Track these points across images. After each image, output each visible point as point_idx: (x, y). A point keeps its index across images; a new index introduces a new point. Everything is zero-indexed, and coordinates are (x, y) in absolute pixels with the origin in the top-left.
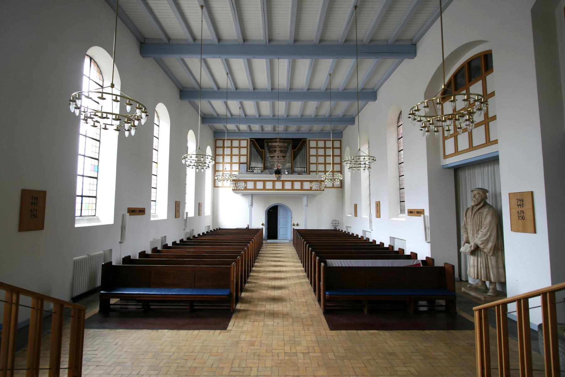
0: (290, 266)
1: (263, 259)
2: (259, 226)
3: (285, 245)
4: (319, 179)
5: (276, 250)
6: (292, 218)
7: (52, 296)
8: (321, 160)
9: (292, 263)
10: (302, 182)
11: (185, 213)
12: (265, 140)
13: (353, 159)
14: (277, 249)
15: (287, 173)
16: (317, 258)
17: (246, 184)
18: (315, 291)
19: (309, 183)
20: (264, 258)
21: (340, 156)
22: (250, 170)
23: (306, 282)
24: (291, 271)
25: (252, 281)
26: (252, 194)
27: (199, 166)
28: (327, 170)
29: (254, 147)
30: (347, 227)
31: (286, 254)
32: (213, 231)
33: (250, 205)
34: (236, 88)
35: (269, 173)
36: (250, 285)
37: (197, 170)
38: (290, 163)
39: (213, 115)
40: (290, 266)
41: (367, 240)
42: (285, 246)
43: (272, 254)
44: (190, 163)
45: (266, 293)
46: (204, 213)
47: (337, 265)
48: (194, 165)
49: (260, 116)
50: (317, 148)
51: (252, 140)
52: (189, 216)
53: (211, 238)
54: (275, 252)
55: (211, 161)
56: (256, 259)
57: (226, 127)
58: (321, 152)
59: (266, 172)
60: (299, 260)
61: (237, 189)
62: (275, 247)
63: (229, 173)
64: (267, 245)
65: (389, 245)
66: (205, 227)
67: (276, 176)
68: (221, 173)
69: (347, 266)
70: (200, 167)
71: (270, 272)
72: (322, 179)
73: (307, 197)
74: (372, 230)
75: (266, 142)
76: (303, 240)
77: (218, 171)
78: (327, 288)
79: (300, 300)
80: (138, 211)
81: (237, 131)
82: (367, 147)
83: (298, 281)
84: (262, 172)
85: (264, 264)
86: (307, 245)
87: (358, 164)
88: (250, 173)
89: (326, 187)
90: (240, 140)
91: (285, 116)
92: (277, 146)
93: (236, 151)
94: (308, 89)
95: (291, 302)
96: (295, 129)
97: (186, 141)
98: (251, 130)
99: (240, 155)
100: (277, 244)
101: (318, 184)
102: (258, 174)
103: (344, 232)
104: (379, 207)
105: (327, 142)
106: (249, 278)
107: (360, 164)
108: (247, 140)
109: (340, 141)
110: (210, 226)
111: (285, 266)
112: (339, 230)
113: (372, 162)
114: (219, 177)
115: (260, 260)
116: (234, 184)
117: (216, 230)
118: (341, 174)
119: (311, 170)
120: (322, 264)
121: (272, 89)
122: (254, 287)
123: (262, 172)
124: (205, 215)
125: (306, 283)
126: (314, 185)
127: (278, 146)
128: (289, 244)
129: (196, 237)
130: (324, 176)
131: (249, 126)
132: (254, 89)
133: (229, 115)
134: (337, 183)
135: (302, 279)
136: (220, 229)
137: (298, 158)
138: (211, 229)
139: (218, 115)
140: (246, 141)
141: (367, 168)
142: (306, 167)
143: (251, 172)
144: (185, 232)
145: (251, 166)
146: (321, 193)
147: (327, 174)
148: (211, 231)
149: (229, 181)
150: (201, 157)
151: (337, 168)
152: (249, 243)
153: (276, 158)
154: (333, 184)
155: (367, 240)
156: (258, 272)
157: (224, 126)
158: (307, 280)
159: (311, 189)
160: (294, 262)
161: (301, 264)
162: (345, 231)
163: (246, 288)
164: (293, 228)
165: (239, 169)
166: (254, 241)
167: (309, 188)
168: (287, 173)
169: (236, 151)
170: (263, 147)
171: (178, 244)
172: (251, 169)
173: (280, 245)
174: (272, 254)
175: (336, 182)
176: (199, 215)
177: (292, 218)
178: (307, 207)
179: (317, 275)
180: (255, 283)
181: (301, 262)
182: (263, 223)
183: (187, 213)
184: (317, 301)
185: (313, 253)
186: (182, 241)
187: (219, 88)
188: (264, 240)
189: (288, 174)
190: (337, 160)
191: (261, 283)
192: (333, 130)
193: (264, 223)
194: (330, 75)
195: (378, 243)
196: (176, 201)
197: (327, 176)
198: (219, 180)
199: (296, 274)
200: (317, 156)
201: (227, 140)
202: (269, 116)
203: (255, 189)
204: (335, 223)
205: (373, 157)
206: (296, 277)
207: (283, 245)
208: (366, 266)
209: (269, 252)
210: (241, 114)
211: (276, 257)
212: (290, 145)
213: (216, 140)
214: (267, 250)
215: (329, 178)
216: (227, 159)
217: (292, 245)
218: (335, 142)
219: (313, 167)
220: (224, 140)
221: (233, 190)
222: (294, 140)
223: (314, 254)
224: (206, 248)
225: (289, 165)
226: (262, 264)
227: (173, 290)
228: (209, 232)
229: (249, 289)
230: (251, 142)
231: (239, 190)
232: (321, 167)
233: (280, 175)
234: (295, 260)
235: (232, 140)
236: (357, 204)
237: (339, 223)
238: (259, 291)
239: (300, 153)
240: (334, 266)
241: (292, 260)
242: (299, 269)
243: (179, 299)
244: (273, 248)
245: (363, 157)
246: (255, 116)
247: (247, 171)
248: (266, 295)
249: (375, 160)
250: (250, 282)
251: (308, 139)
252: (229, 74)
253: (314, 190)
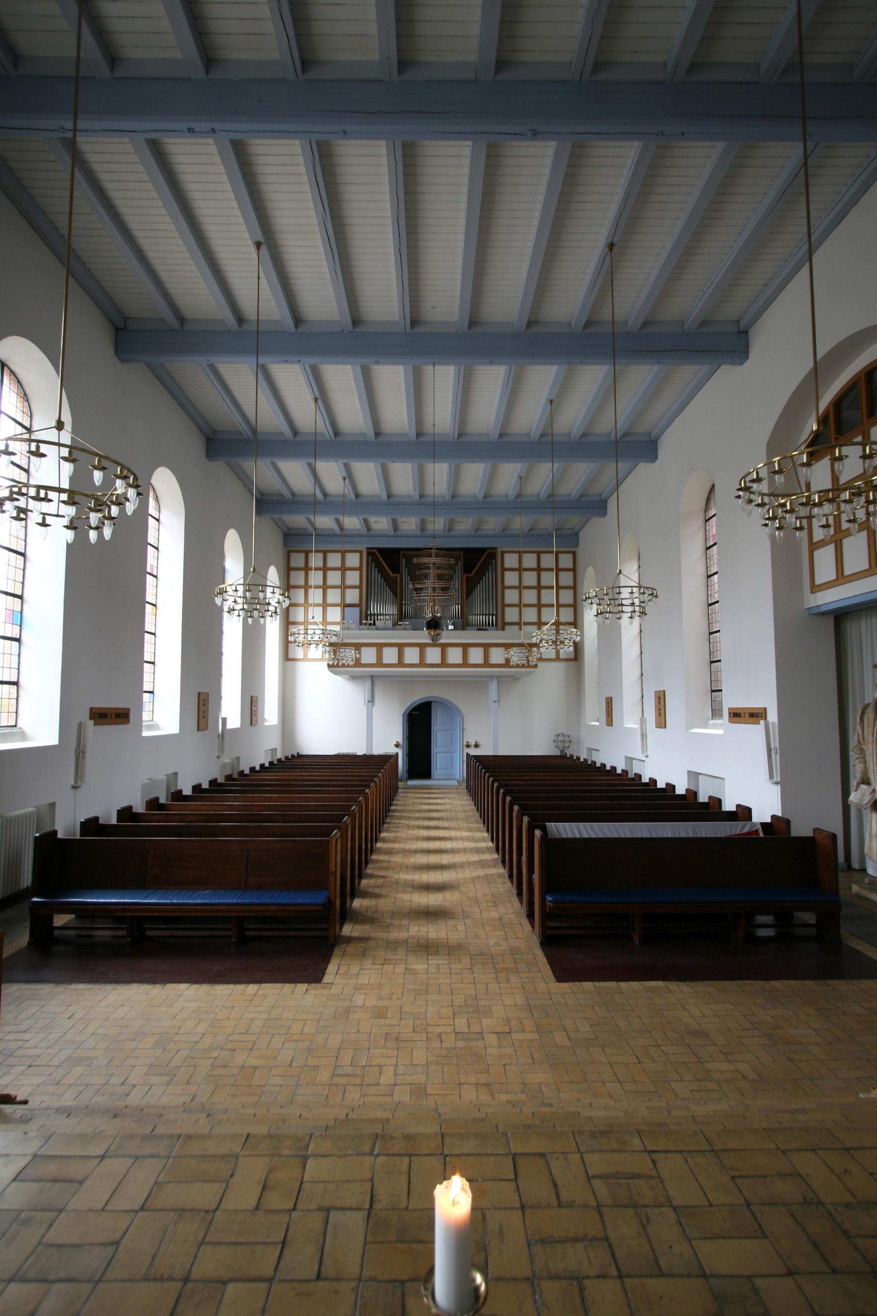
0: (462, 839)
1: (399, 823)
2: (392, 750)
3: (448, 791)
4: (526, 641)
5: (429, 804)
6: (465, 731)
8: (530, 597)
9: (466, 831)
10: (486, 647)
11: (220, 721)
12: (401, 553)
13: (607, 594)
14: (431, 801)
15: (451, 627)
16: (526, 819)
17: (360, 653)
18: (519, 894)
19: (502, 650)
20: (403, 821)
21: (574, 588)
22: (367, 620)
23: (499, 875)
24: (464, 851)
25: (376, 873)
26: (372, 677)
27: (255, 612)
28: (543, 620)
29: (376, 567)
30: (590, 750)
31: (451, 811)
32: (283, 759)
33: (369, 701)
34: (337, 433)
35: (410, 627)
36: (372, 881)
37: (250, 620)
38: (458, 604)
39: (282, 495)
40: (462, 839)
41: (637, 778)
42: (450, 793)
43: (420, 811)
44: (234, 604)
45: (409, 899)
46: (264, 720)
47: (570, 836)
48: (243, 609)
49: (389, 496)
50: (520, 570)
51: (371, 552)
52: (228, 727)
53: (279, 775)
54: (427, 807)
55: (281, 598)
56: (383, 824)
57: (312, 524)
58: (530, 579)
59: (405, 625)
60: (482, 825)
61: (338, 664)
62: (427, 796)
63: (321, 627)
64: (407, 793)
65: (687, 790)
66: (265, 751)
67: (430, 634)
68: (302, 627)
69: (593, 836)
70: (256, 613)
71: (416, 851)
72: (534, 640)
73: (498, 682)
74: (647, 756)
76: (491, 779)
77: (294, 623)
78: (547, 889)
79: (486, 915)
80: (114, 715)
81: (338, 531)
82: (636, 566)
83: (481, 872)
84: (395, 624)
85: (403, 833)
86: (502, 791)
87: (617, 604)
88: (367, 627)
89: (541, 659)
90: (343, 553)
91: (448, 497)
92: (431, 565)
93: (334, 578)
94: (501, 435)
95: (466, 920)
96: (469, 527)
97: (222, 557)
98: (369, 529)
99: (343, 587)
100: (429, 789)
101: (524, 651)
102: (386, 629)
103: (582, 760)
104: (662, 703)
105: (543, 556)
106: (369, 866)
107: (622, 605)
108: (361, 552)
109: (574, 554)
110: (276, 749)
111: (450, 839)
112: (572, 756)
113: (649, 600)
114: (297, 635)
115: (392, 825)
116: (332, 653)
117: (290, 757)
118: (576, 628)
119: (507, 620)
120: (538, 833)
121: (419, 435)
122: (382, 886)
123: (395, 624)
124: (266, 724)
125: (500, 877)
126: (516, 654)
127: (434, 564)
128: (456, 789)
129: (246, 775)
130: (539, 633)
131: (366, 521)
132: (377, 434)
133: (319, 495)
134: (567, 650)
135: (489, 867)
136: (300, 756)
137: (478, 593)
138: (279, 755)
139: (294, 495)
141: (637, 614)
142: (495, 613)
143: (370, 624)
144: (220, 763)
145: (369, 612)
146: (531, 673)
147: (545, 628)
148: (279, 760)
149: (321, 646)
150: (260, 591)
151: (567, 615)
152: (368, 786)
153: (430, 591)
154: (558, 653)
155: (637, 778)
156: (390, 852)
157: (309, 520)
158: (501, 870)
159: (507, 664)
160: (470, 830)
161: (486, 835)
162: (584, 759)
163: (363, 890)
164: (467, 753)
165: (343, 618)
166: (380, 781)
167: (502, 662)
168: (453, 627)
169: (334, 578)
170: (396, 569)
171: (205, 791)
172: (369, 618)
173: (437, 791)
174: (420, 811)
175: (566, 648)
176: (251, 724)
177: (463, 729)
178: (499, 705)
179: (524, 858)
180: (384, 877)
181: (485, 829)
182: (397, 742)
183: (224, 720)
184: (526, 917)
185: (516, 808)
186: (213, 782)
187: (295, 433)
188: (401, 781)
189: (455, 629)
190: (567, 597)
191: (397, 876)
192: (557, 530)
193: (401, 741)
194: (551, 402)
195: (661, 785)
196: (199, 693)
197: (546, 632)
198: (299, 643)
199: (475, 858)
200: (520, 588)
201: (316, 551)
202: (411, 496)
203: (379, 663)
204: (563, 742)
205: (653, 589)
206: (474, 863)
207: (445, 791)
208: (636, 836)
209: (414, 809)
210: (346, 493)
211: (429, 819)
212: (460, 562)
213: (289, 553)
214: (407, 802)
215: (550, 638)
216: (315, 596)
217: (465, 790)
218: (561, 556)
219: (511, 615)
220: (307, 553)
221: (329, 666)
222: (467, 551)
223: (518, 810)
224: (270, 799)
225: (456, 609)
226: (399, 834)
227: (199, 893)
228: (275, 762)
229: (370, 890)
231: (343, 666)
232: (530, 615)
233: (438, 631)
234: (472, 825)
235: (325, 553)
236: (611, 698)
237: (570, 742)
238: (394, 895)
240: (564, 836)
241: (466, 825)
242: (483, 845)
243: (211, 914)
244: (422, 798)
245: (629, 590)
246: (379, 496)
247: (361, 623)
248: (409, 903)
249: (656, 596)
250: (372, 876)
251: (499, 550)
252: (320, 402)
253: (515, 664)
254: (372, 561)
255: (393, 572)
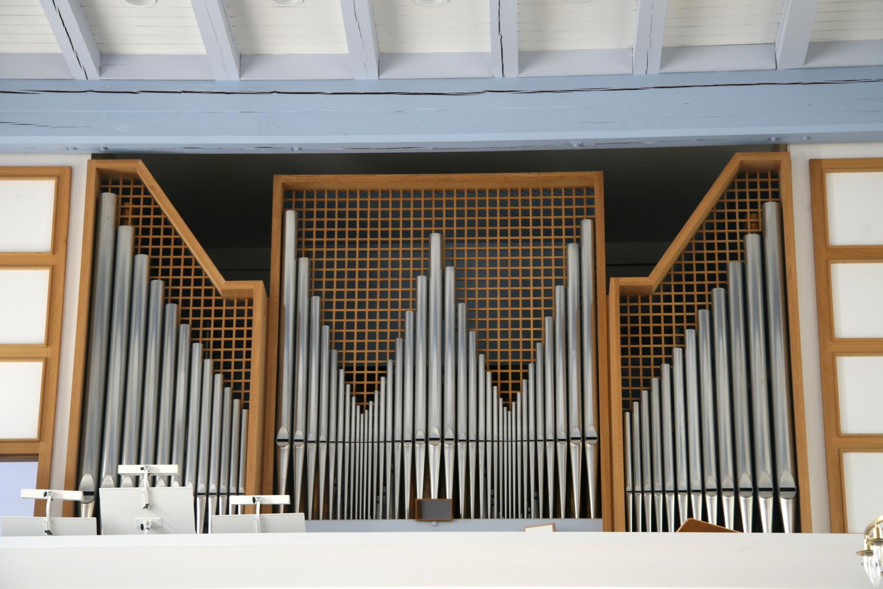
7: (597, 172)
12: (279, 182)
75: (292, 197)
88: (44, 522)
140: (49, 186)
142: (786, 479)
212: (587, 226)
230: (109, 199)
239: (702, 316)
254: (120, 221)
255: (228, 274)
